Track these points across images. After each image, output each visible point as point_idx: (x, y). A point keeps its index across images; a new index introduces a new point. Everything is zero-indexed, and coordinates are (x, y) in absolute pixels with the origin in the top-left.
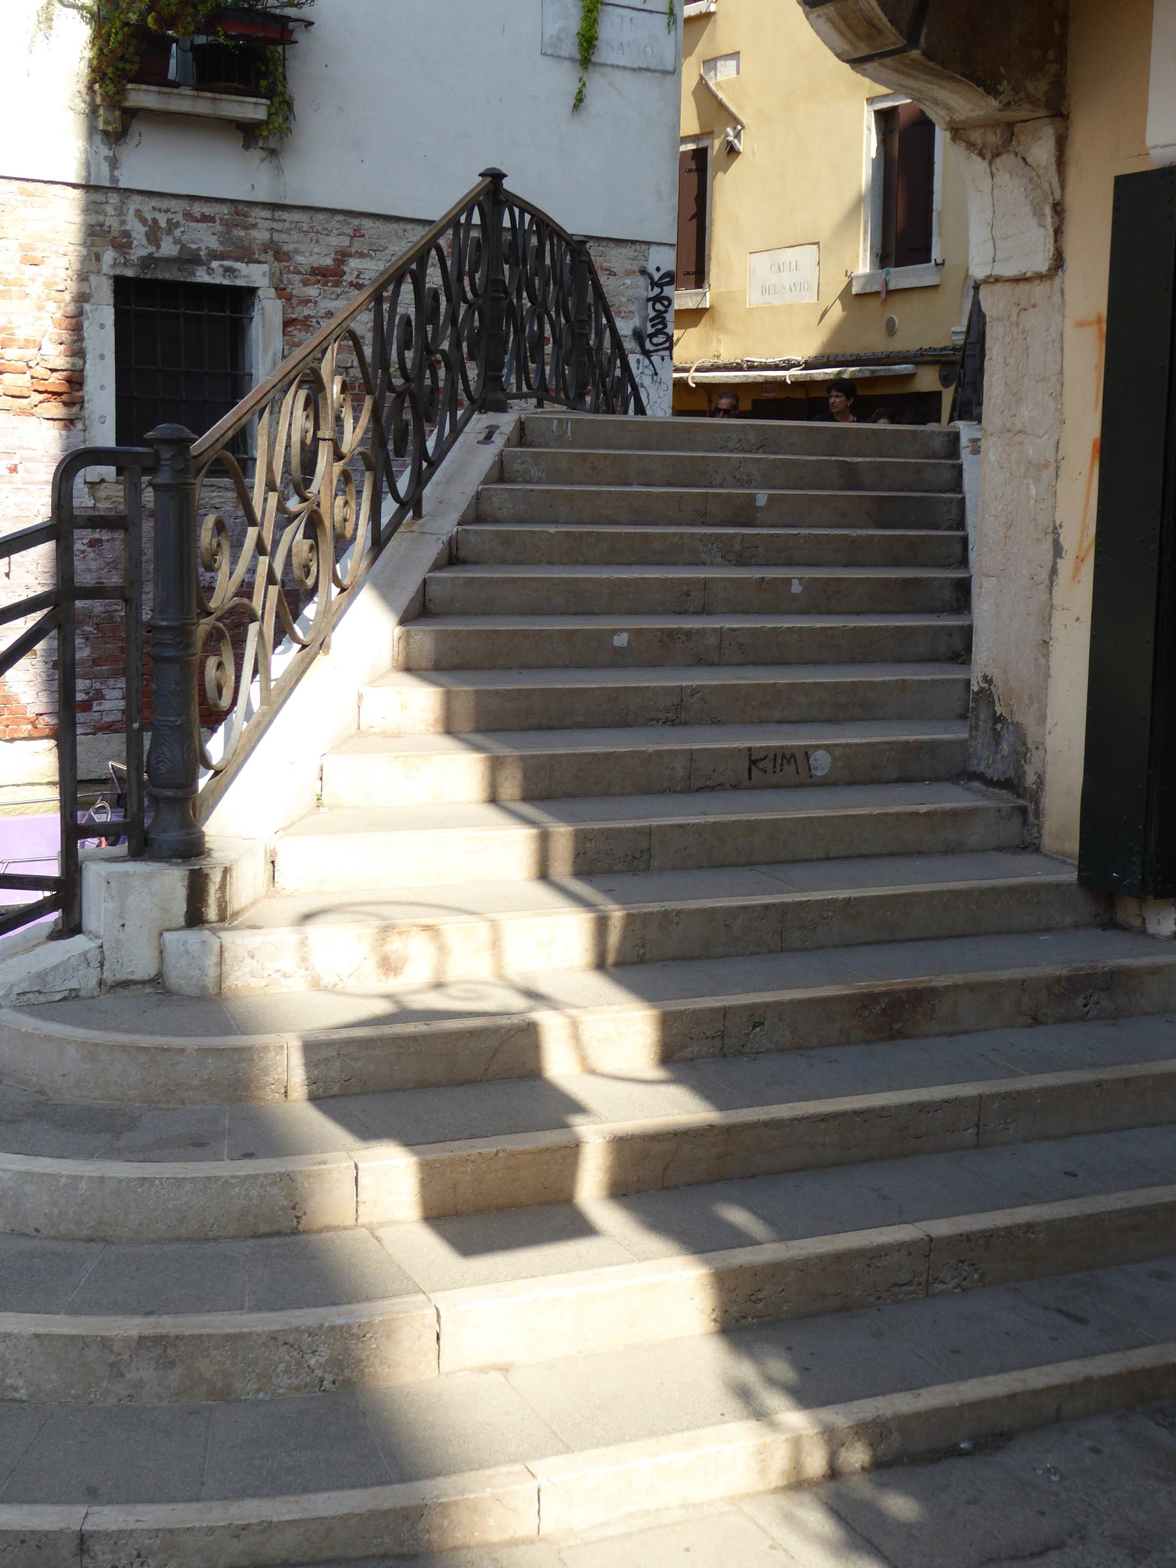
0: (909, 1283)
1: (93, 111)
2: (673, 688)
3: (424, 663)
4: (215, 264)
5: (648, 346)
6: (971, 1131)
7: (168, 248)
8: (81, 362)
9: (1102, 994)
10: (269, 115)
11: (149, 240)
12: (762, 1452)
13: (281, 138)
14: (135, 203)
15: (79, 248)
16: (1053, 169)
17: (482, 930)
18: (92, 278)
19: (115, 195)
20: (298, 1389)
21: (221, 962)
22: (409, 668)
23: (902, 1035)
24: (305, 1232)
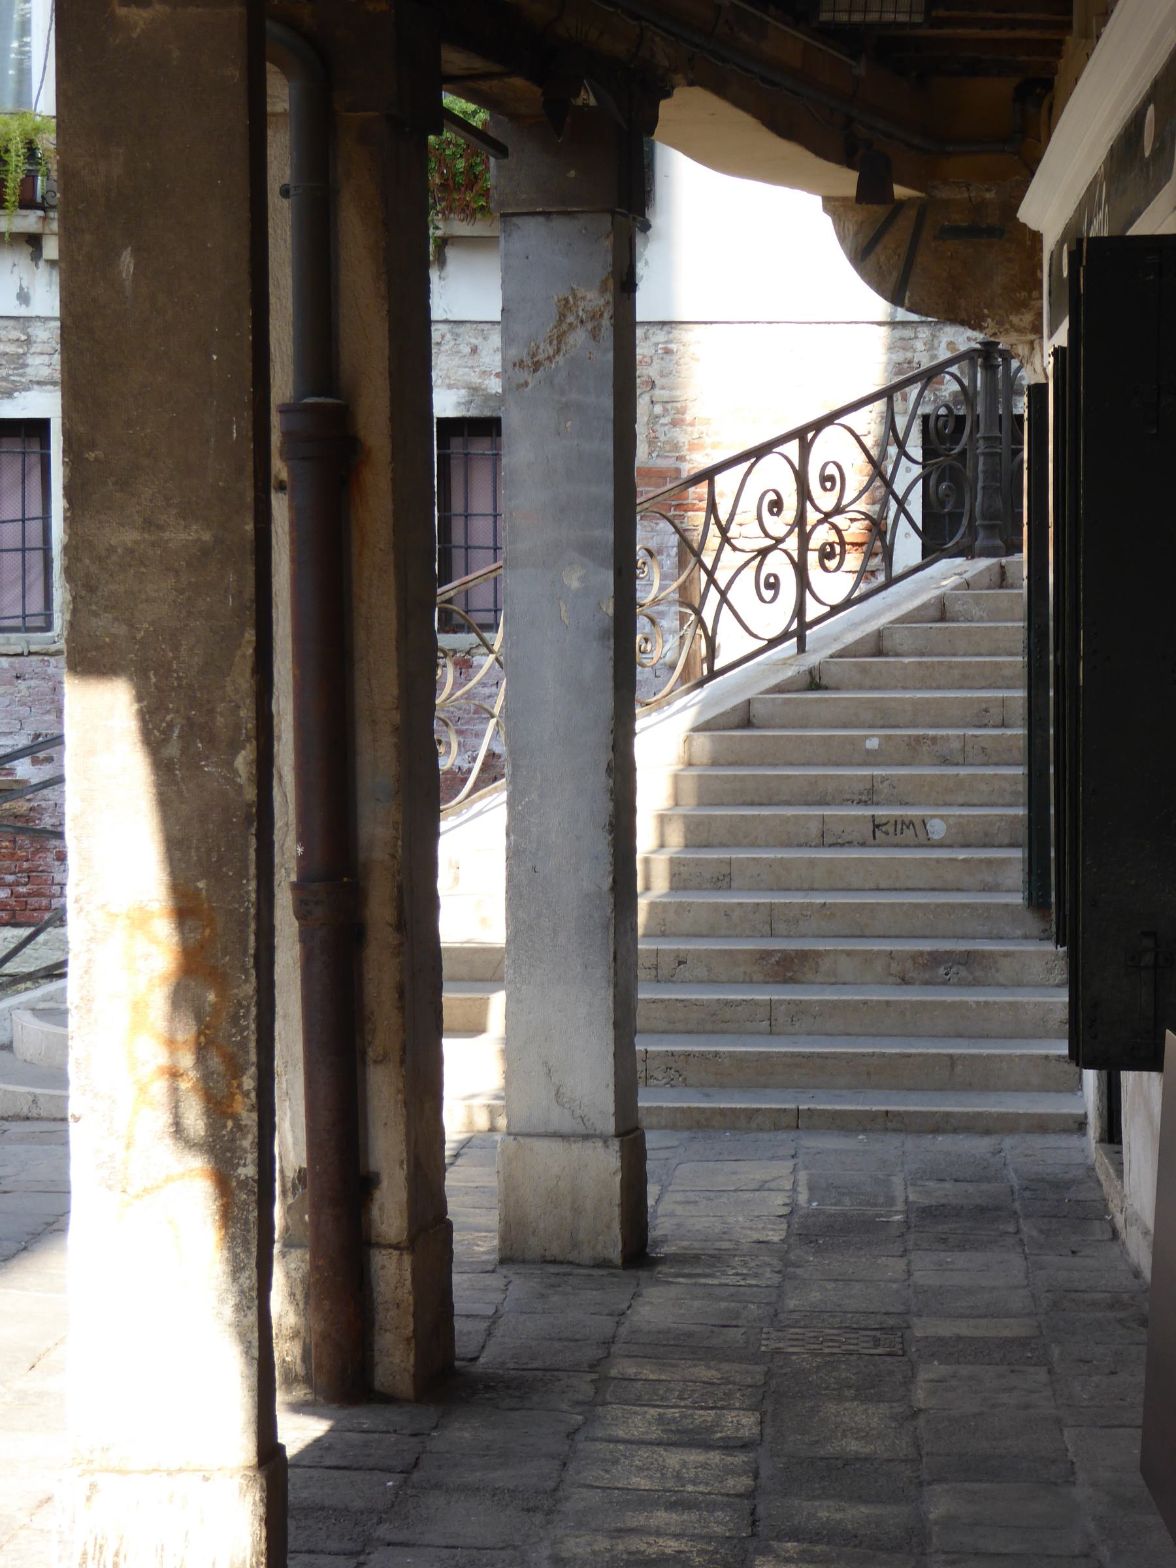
2: (865, 776)
6: (766, 1023)
9: (961, 967)
19: (925, 329)
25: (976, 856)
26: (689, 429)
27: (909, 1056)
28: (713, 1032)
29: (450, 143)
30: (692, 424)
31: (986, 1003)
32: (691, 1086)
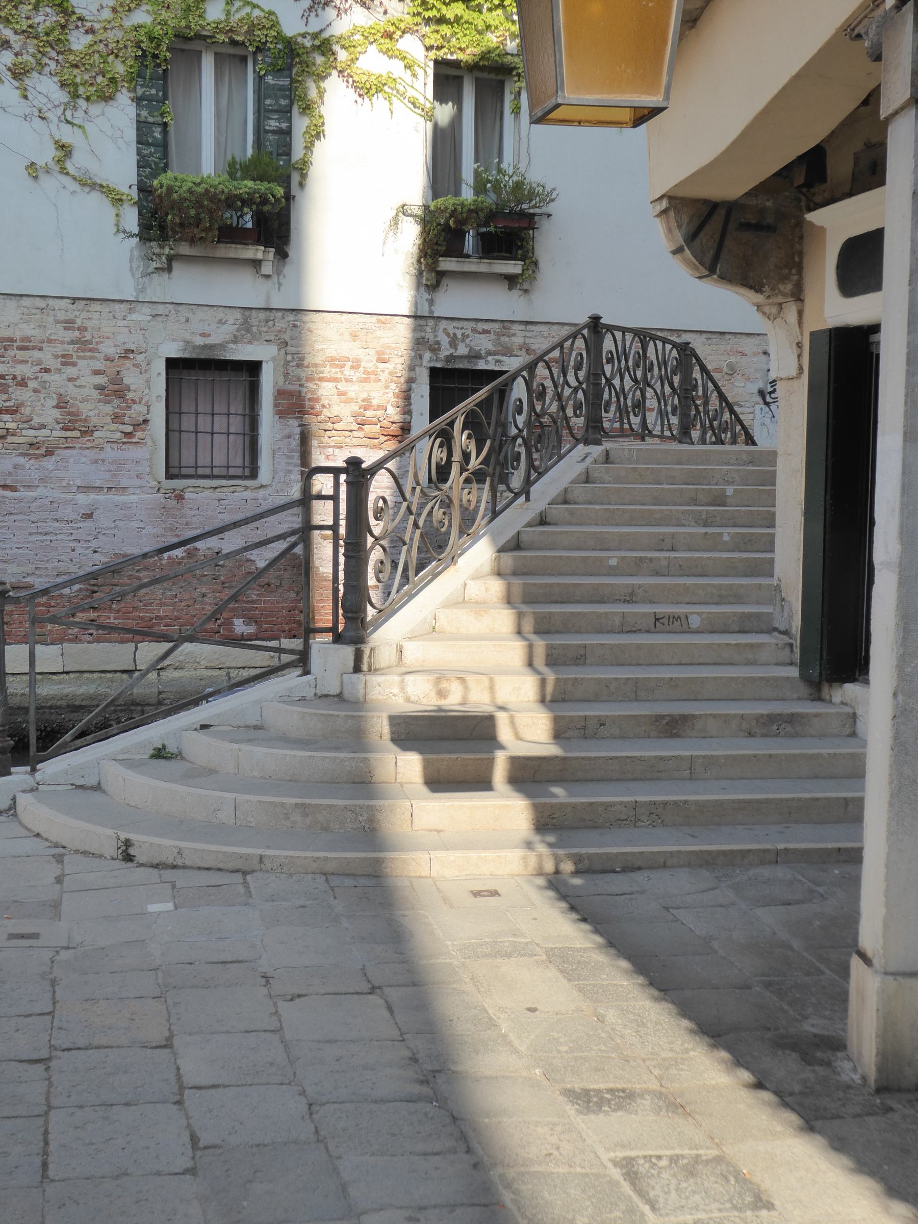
0: (626, 820)
1: (420, 273)
3: (508, 571)
4: (490, 358)
5: (768, 399)
7: (462, 350)
8: (409, 418)
10: (523, 270)
11: (451, 346)
12: (525, 858)
13: (531, 283)
14: (443, 324)
15: (410, 352)
16: (797, 325)
17: (485, 681)
18: (417, 369)
20: (355, 829)
21: (365, 688)
22: (499, 574)
23: (676, 736)
24: (374, 783)
25: (743, 642)
26: (306, 369)
27: (818, 799)
28: (651, 779)
29: (186, 199)
30: (308, 367)
31: (835, 754)
32: (666, 826)
